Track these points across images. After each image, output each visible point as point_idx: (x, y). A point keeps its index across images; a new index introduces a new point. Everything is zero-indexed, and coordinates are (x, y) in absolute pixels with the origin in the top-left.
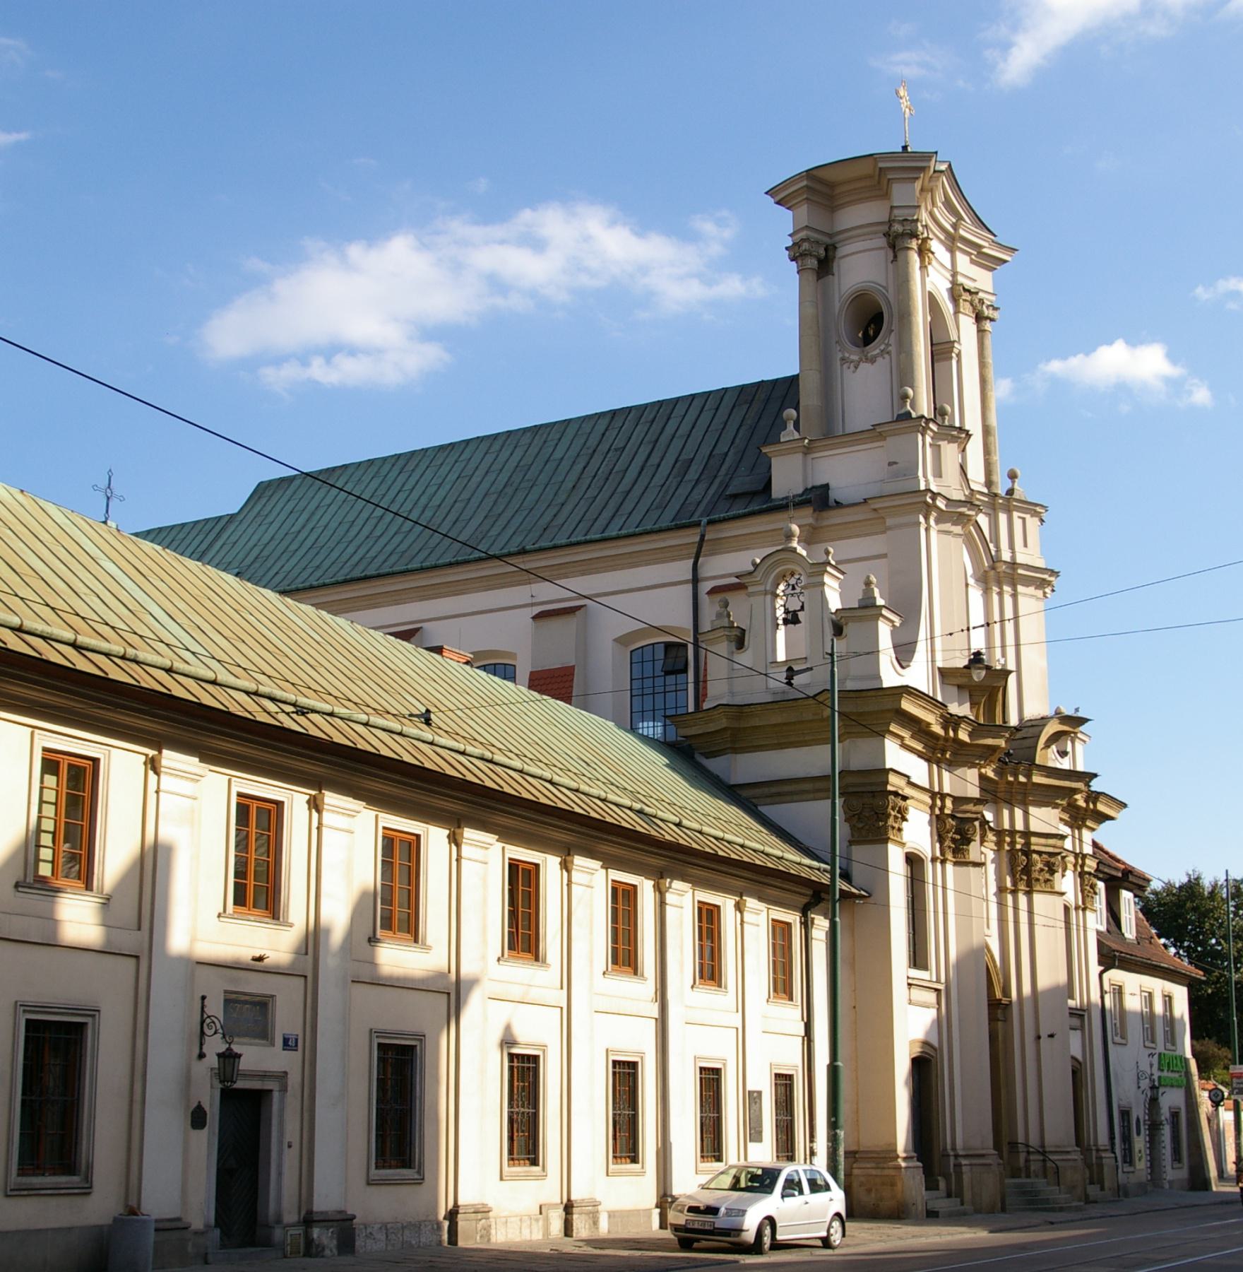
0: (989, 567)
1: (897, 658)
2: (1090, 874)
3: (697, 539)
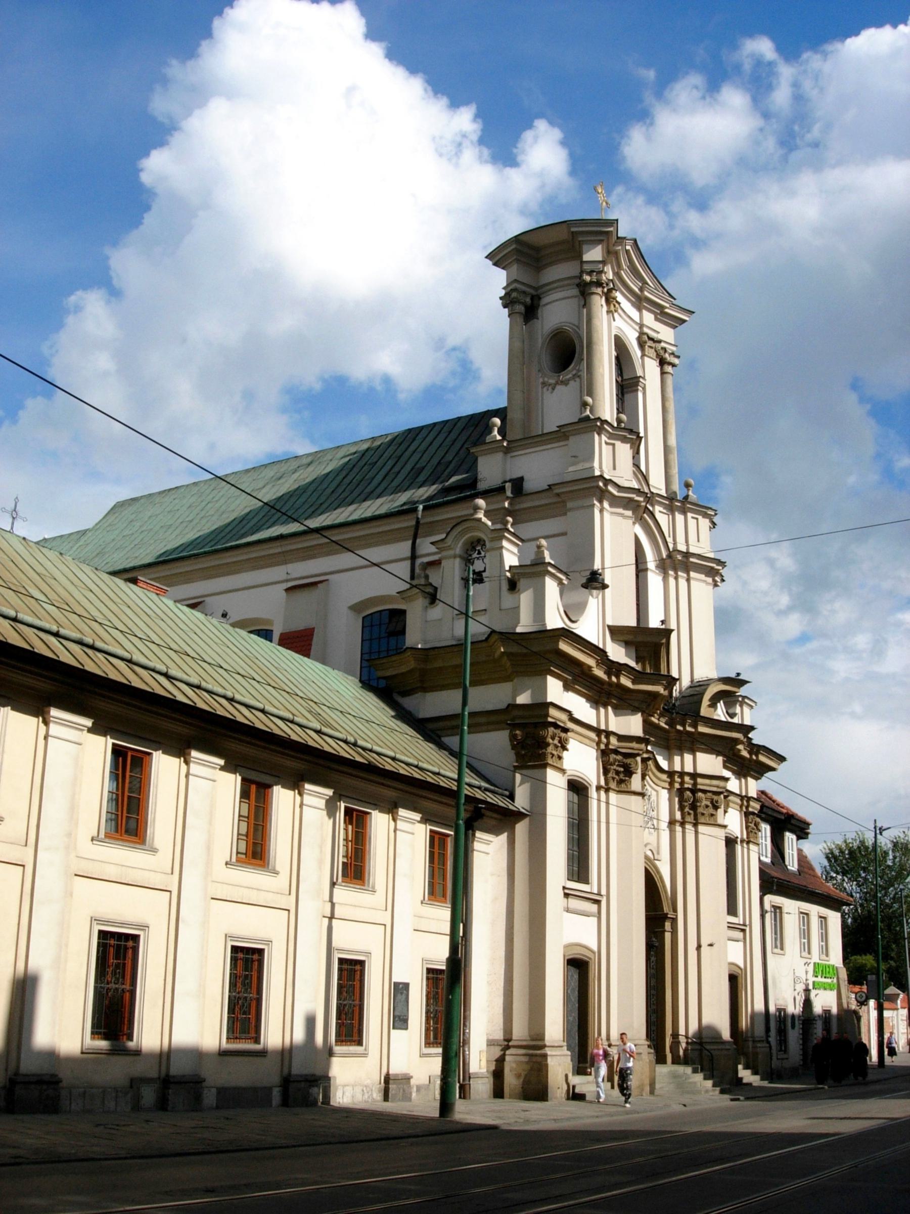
1: (565, 612)
2: (753, 814)
3: (413, 523)
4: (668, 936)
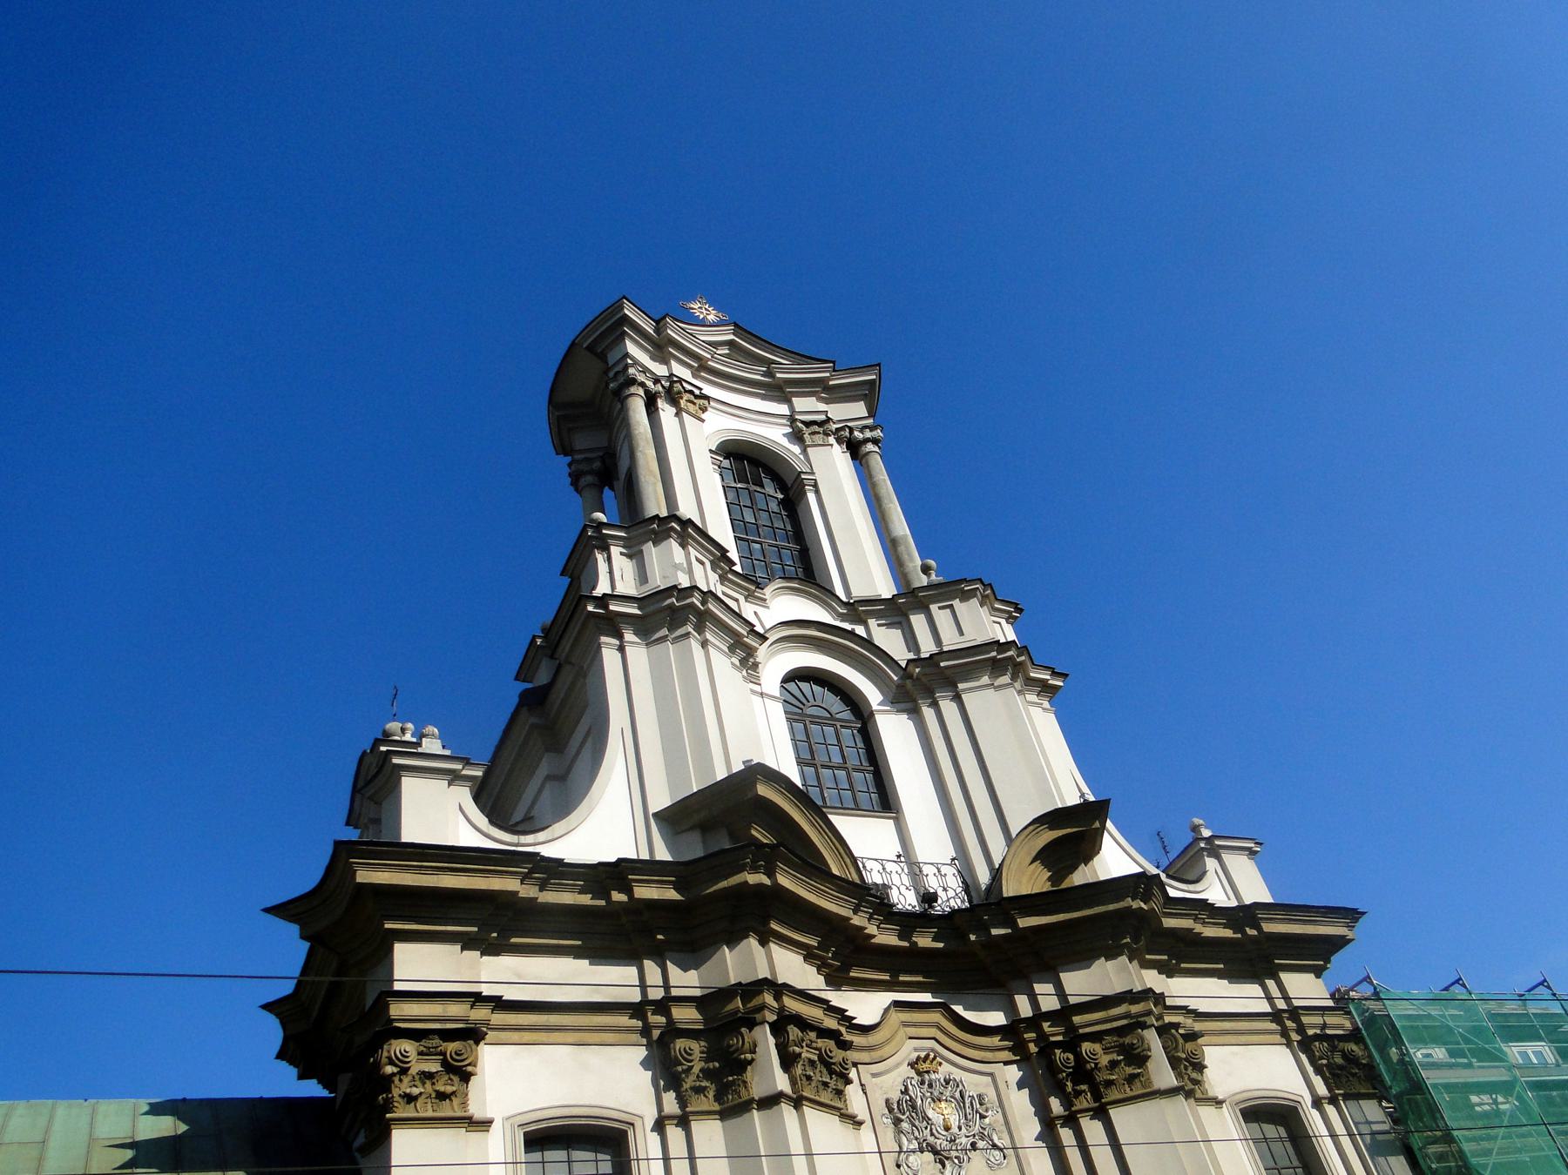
0: (901, 678)
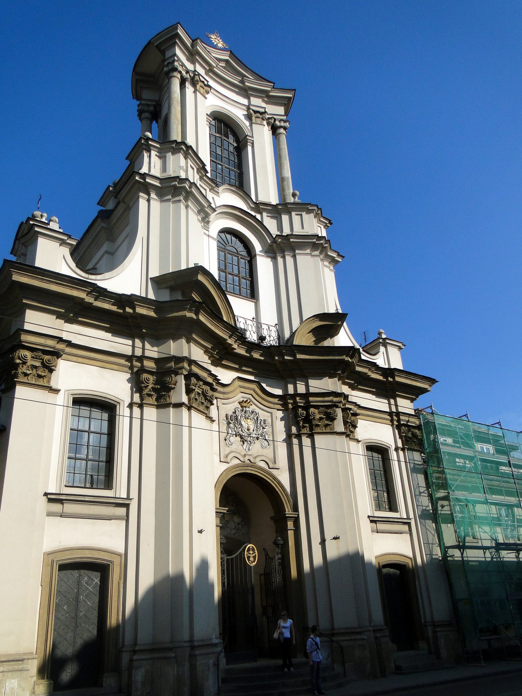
4: (291, 534)
